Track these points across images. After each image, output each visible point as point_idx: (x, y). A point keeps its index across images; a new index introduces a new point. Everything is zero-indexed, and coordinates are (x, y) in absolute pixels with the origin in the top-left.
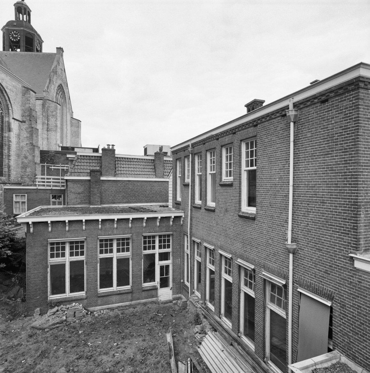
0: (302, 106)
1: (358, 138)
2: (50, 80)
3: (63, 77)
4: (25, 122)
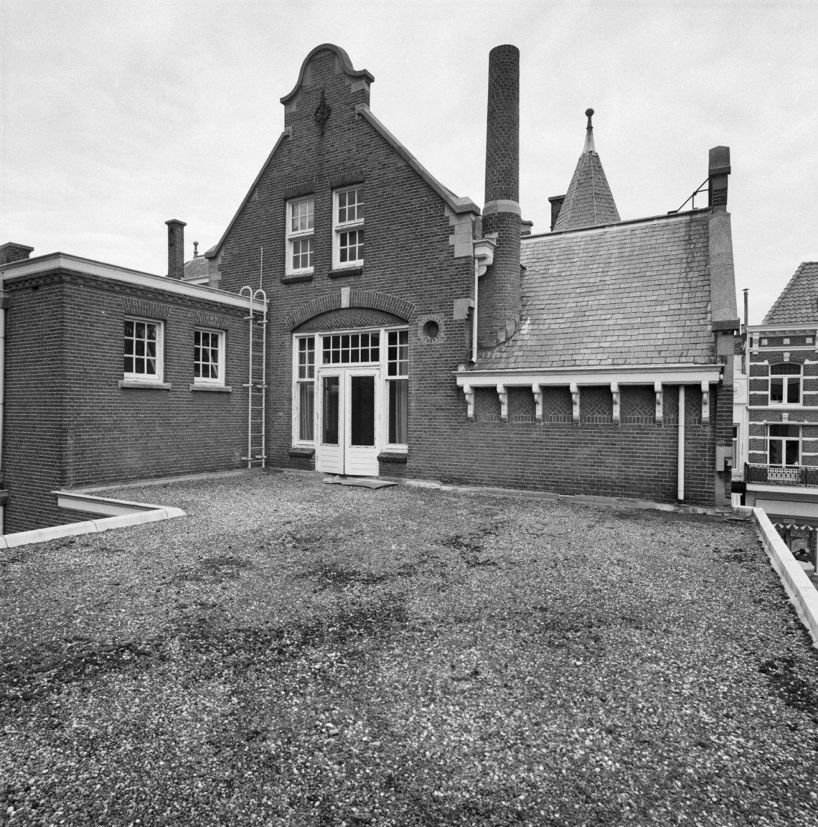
0: (14, 288)
1: (62, 344)
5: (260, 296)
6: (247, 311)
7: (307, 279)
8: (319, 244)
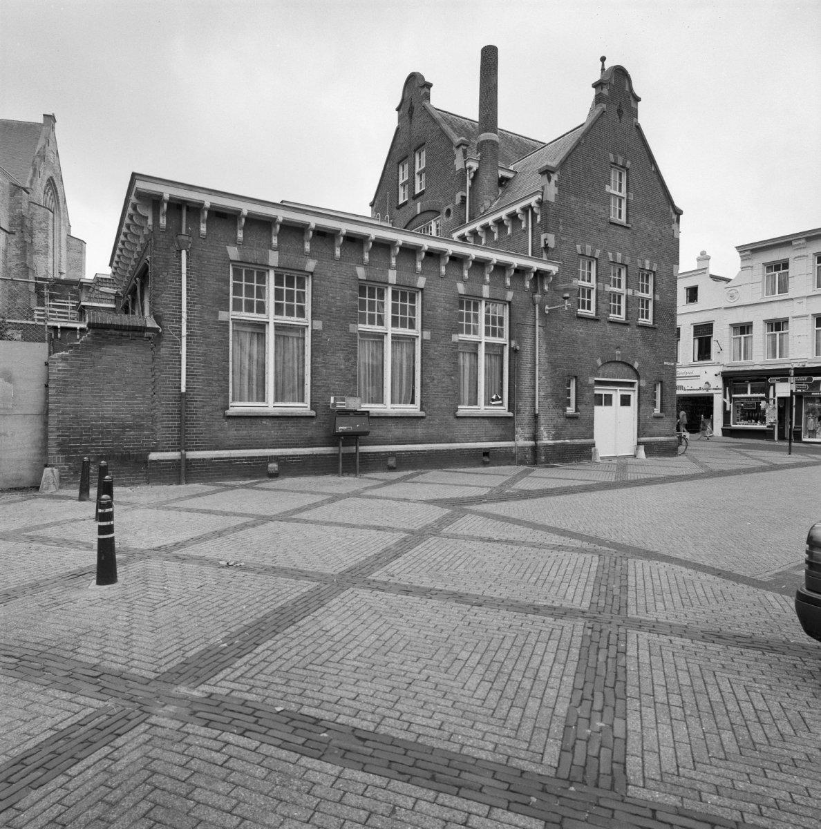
2: (35, 170)
3: (55, 165)
4: (14, 234)
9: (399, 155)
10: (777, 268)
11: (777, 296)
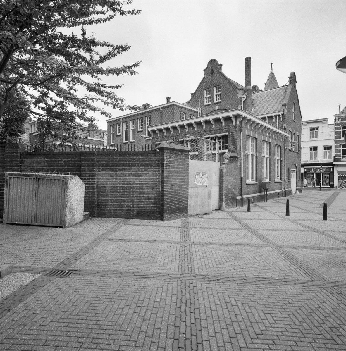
5: (200, 109)
6: (198, 112)
7: (209, 105)
8: (211, 98)
9: (203, 86)
10: (314, 129)
11: (314, 139)
